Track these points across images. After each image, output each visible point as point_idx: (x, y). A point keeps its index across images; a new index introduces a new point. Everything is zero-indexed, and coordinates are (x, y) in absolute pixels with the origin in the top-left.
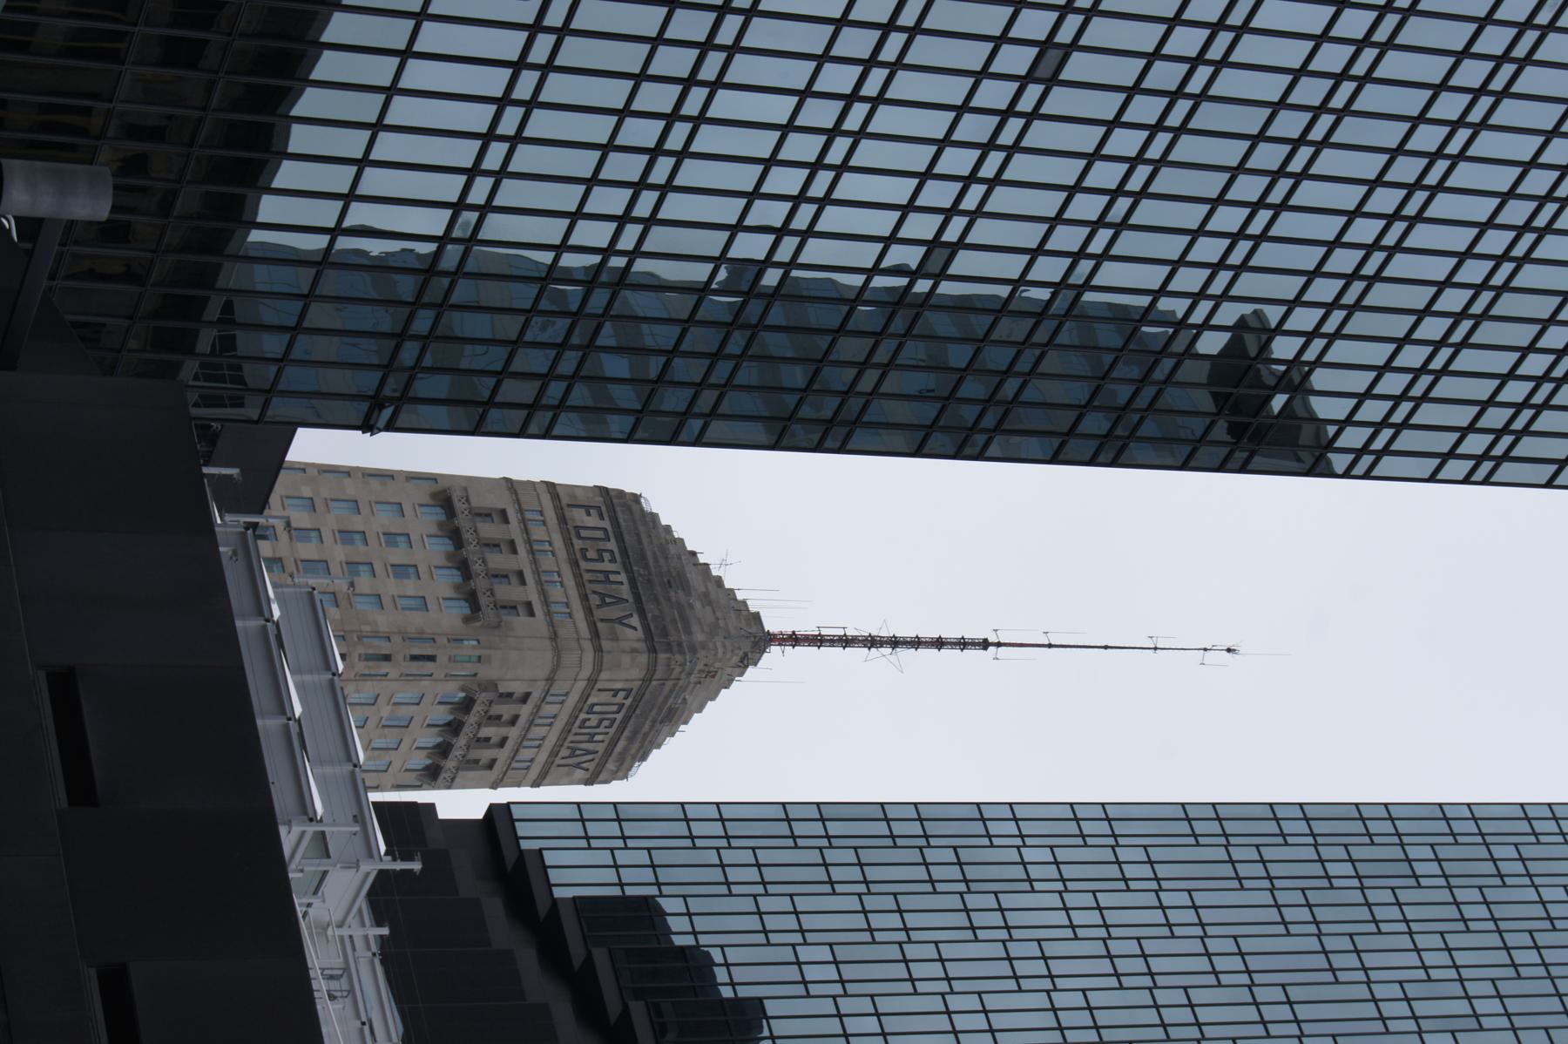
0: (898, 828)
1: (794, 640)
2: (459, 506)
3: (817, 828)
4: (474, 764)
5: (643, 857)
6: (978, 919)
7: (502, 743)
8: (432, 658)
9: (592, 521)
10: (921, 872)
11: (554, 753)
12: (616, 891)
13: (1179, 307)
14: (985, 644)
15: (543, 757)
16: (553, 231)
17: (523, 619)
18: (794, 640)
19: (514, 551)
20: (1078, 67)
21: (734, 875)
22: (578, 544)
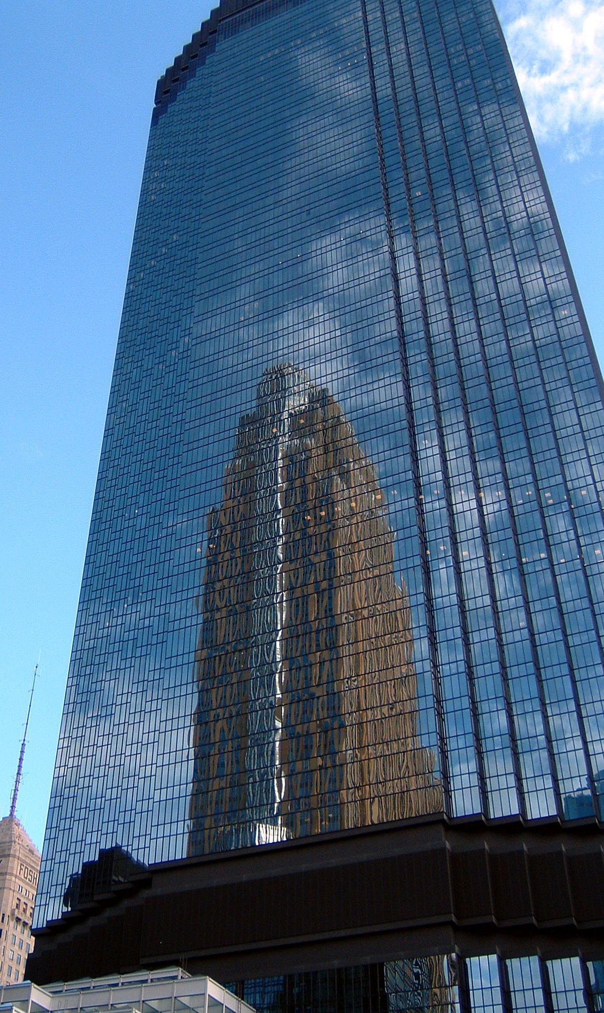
1: (13, 807)
21: (78, 850)
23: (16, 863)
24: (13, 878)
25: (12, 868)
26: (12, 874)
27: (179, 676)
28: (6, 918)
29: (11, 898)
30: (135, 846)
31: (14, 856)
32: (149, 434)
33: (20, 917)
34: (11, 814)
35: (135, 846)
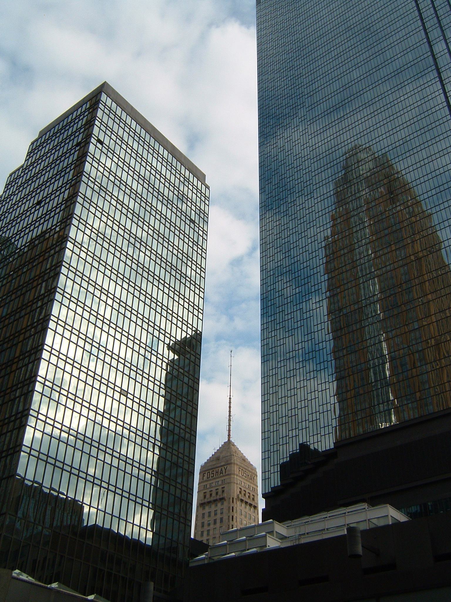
0: (266, 417)
1: (229, 435)
2: (203, 502)
3: (266, 433)
4: (253, 499)
5: (272, 467)
6: (283, 402)
7: (249, 493)
8: (233, 516)
9: (206, 475)
10: (275, 413)
11: (251, 483)
12: (279, 473)
13: (164, 364)
14: (230, 398)
15: (252, 485)
16: (147, 486)
17: (225, 489)
18: (229, 435)
19: (212, 491)
20: (125, 387)
21: (275, 449)
22: (210, 478)
23: (236, 467)
24: (236, 476)
25: (234, 470)
26: (234, 474)
27: (328, 104)
28: (235, 500)
29: (236, 489)
30: (312, 442)
31: (234, 464)
32: (274, 192)
33: (242, 498)
34: (229, 440)
35: (312, 442)
